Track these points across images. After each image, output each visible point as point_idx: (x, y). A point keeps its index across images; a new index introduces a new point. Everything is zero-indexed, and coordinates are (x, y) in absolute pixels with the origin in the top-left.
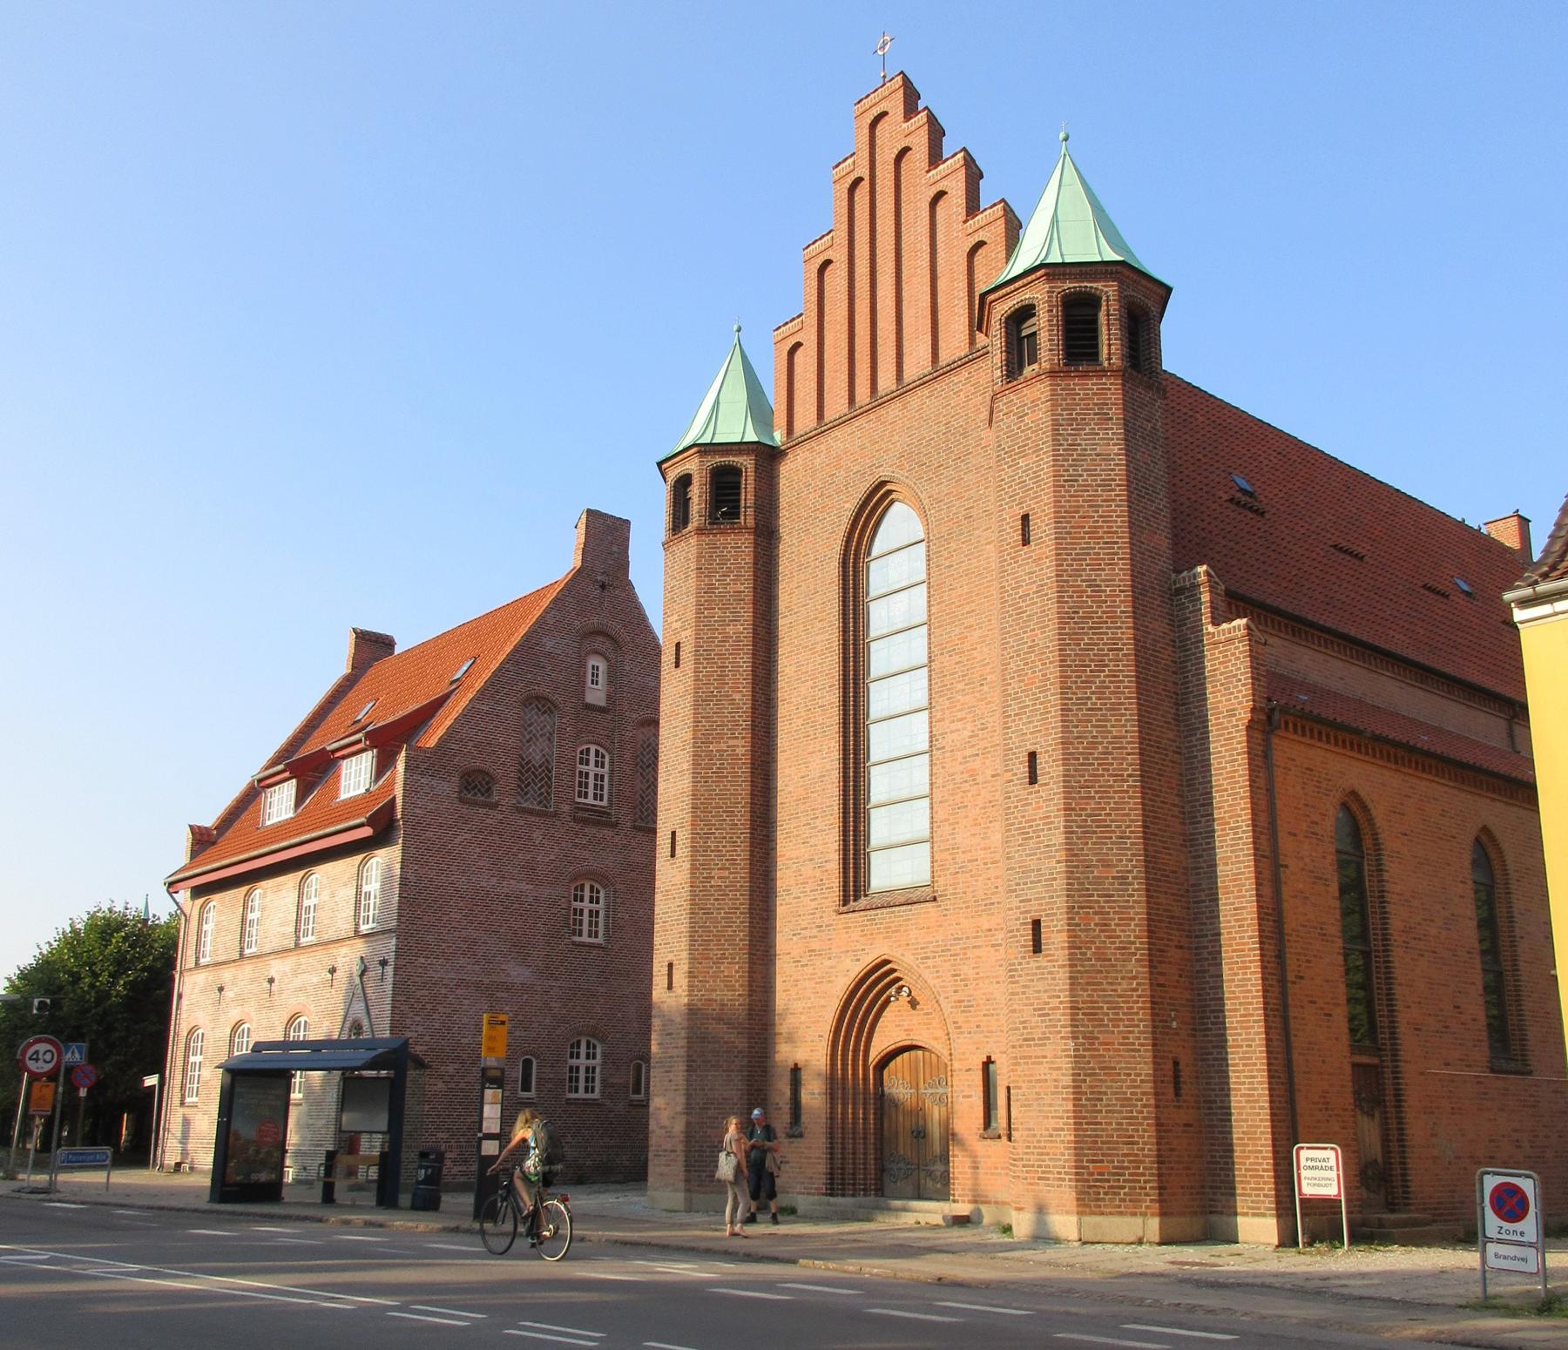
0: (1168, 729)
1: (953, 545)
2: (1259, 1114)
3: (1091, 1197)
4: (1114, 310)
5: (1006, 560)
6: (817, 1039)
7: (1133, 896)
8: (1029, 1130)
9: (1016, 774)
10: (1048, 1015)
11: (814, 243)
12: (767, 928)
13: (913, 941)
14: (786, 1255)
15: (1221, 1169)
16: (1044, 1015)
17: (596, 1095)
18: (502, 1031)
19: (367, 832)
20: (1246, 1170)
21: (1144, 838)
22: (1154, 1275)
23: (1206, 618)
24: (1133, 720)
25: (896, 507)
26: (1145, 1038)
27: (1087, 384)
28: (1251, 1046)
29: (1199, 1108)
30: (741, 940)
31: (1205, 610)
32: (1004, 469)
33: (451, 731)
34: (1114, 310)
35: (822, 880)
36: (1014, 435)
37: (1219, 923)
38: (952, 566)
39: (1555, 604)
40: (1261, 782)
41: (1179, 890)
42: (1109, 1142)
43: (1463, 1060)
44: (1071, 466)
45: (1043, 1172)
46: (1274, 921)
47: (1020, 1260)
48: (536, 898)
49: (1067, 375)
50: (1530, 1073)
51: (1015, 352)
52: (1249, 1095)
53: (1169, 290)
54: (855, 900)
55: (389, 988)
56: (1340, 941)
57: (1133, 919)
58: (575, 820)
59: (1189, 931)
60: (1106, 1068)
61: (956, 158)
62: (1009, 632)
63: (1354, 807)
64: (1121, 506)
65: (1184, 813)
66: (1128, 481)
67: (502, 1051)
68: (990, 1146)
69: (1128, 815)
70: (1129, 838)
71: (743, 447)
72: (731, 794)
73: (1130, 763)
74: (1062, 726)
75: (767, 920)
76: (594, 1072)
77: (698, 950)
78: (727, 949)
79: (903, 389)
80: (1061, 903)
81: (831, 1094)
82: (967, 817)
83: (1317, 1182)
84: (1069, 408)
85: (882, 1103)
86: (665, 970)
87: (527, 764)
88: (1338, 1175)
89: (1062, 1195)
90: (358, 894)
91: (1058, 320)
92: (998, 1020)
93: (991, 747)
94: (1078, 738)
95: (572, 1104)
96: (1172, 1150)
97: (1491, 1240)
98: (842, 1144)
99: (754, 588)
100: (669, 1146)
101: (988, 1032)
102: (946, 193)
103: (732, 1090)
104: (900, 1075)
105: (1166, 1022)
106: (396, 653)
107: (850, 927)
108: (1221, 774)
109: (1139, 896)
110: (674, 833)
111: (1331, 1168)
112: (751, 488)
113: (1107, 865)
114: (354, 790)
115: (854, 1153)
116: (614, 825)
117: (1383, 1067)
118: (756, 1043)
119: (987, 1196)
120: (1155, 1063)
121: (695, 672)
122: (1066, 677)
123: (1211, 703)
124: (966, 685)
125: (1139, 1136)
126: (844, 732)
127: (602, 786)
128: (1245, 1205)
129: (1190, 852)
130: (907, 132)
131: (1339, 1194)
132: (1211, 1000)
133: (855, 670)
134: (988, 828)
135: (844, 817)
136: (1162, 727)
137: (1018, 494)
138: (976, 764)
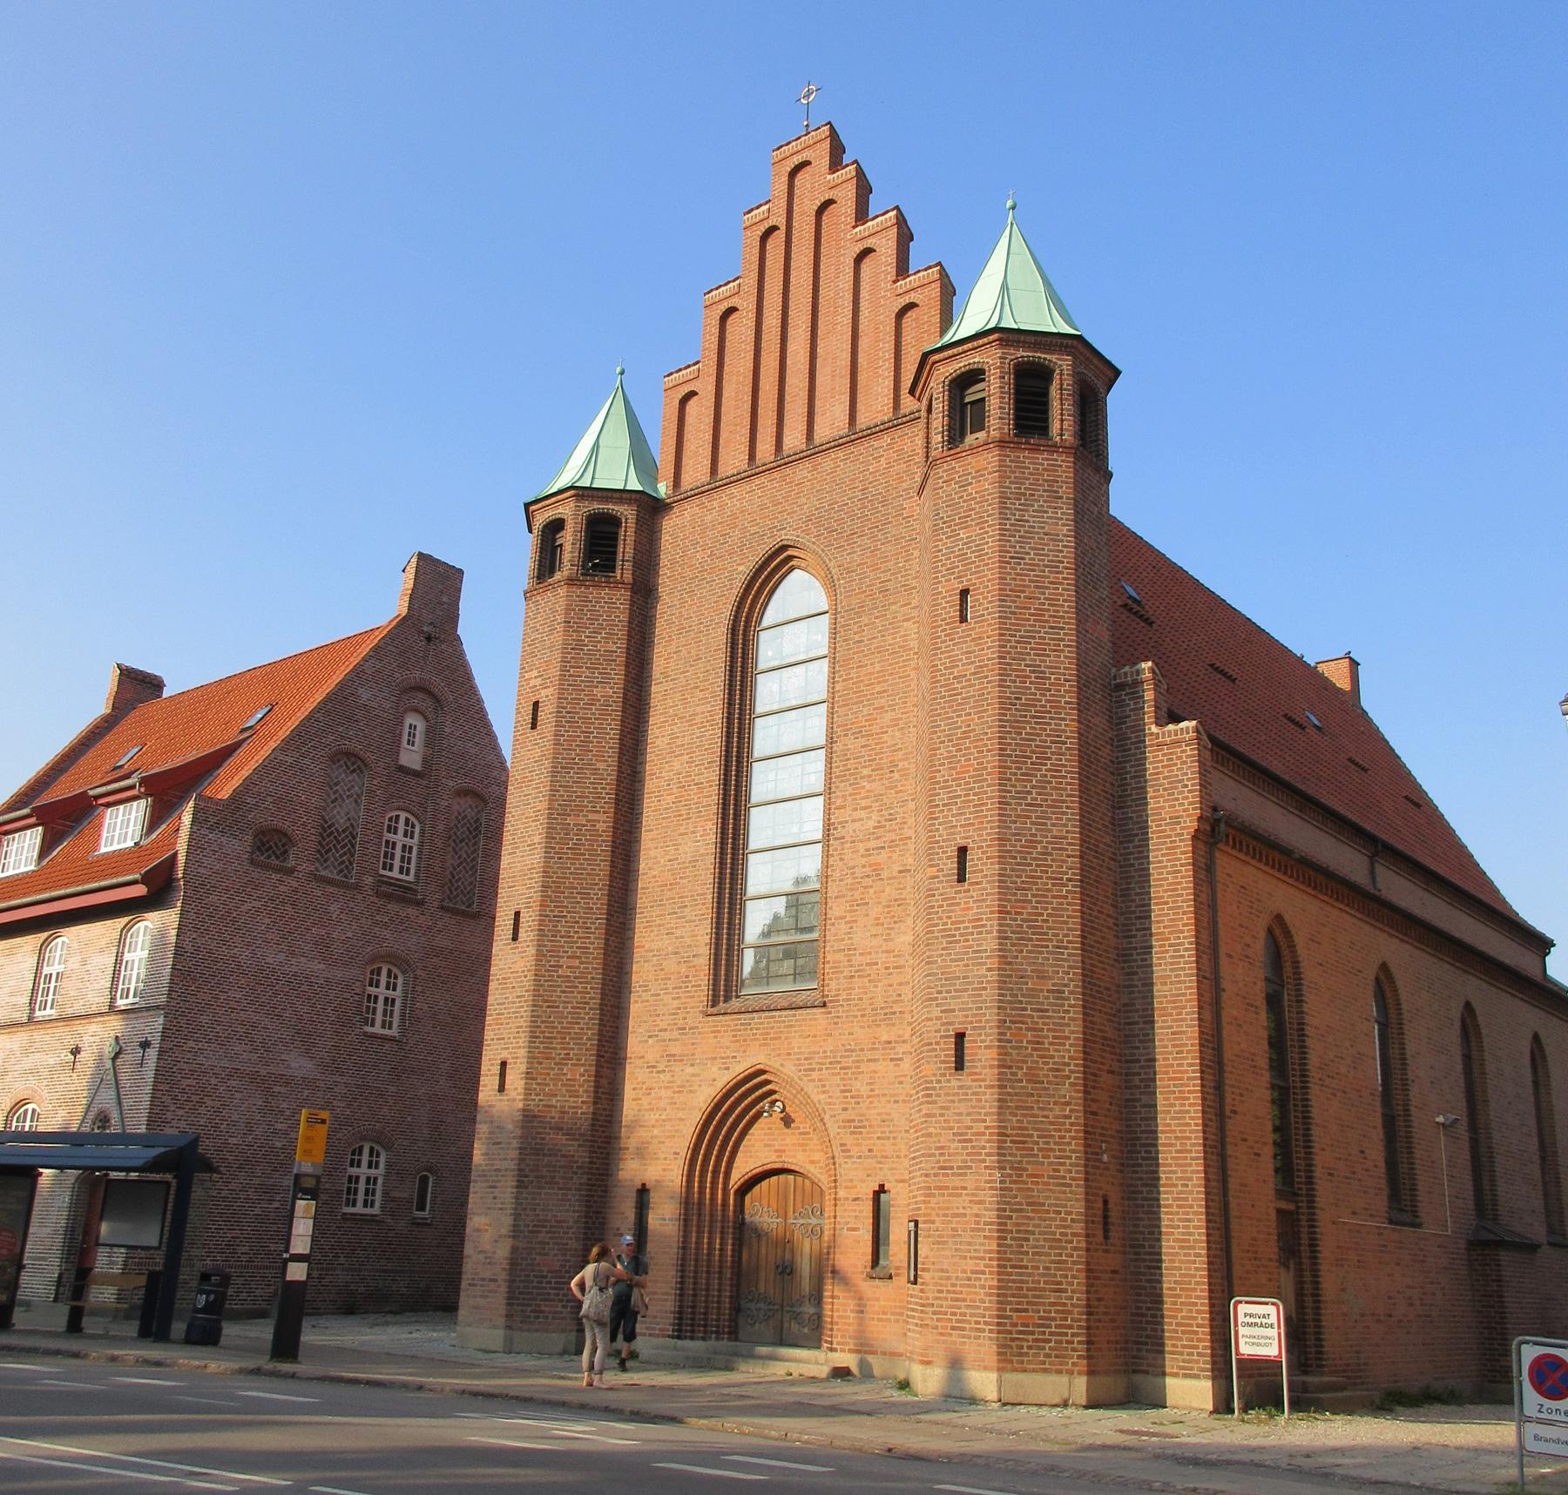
1: (865, 620)
2: (1195, 1262)
3: (1011, 1355)
4: (1068, 385)
5: (939, 637)
6: (672, 1157)
7: (1068, 1012)
8: (942, 1271)
12: (617, 1028)
15: (1147, 1322)
16: (965, 1141)
17: (376, 1210)
18: (323, 1130)
19: (140, 890)
20: (1177, 1324)
23: (1149, 718)
25: (797, 574)
27: (1038, 459)
28: (1187, 1186)
30: (588, 1039)
31: (1149, 709)
33: (248, 784)
35: (687, 977)
37: (1154, 1047)
40: (1203, 898)
41: (1111, 1008)
42: (1035, 1289)
43: (1366, 1209)
44: (1018, 542)
46: (1213, 1049)
47: (948, 1424)
48: (327, 980)
49: (1017, 446)
50: (1419, 1226)
51: (958, 418)
53: (1117, 373)
54: (725, 1002)
55: (150, 1074)
57: (1069, 1038)
58: (378, 894)
59: (1120, 1055)
61: (887, 216)
62: (939, 715)
63: (1277, 932)
66: (1076, 564)
67: (319, 1156)
69: (1066, 923)
71: (624, 496)
73: (1070, 867)
74: (1000, 821)
77: (538, 1048)
78: (573, 1049)
79: (813, 450)
80: (990, 1016)
81: (685, 1220)
82: (867, 915)
83: (1255, 1340)
85: (742, 1230)
86: (497, 1069)
87: (330, 827)
89: (981, 1348)
90: (118, 961)
91: (1009, 388)
94: (1016, 834)
95: (348, 1219)
97: (1529, 1420)
100: (487, 1275)
101: (883, 1157)
102: (875, 251)
103: (567, 1211)
104: (765, 1202)
106: (164, 696)
107: (719, 1032)
108: (1162, 885)
109: (1075, 1012)
110: (517, 914)
111: (1272, 1326)
112: (630, 540)
113: (1042, 977)
114: (119, 843)
115: (707, 1290)
116: (420, 903)
119: (872, 1346)
120: (1087, 1201)
122: (1004, 767)
123: (1152, 809)
124: (873, 771)
128: (1175, 1364)
130: (832, 184)
134: (893, 929)
137: (958, 567)
138: (882, 857)
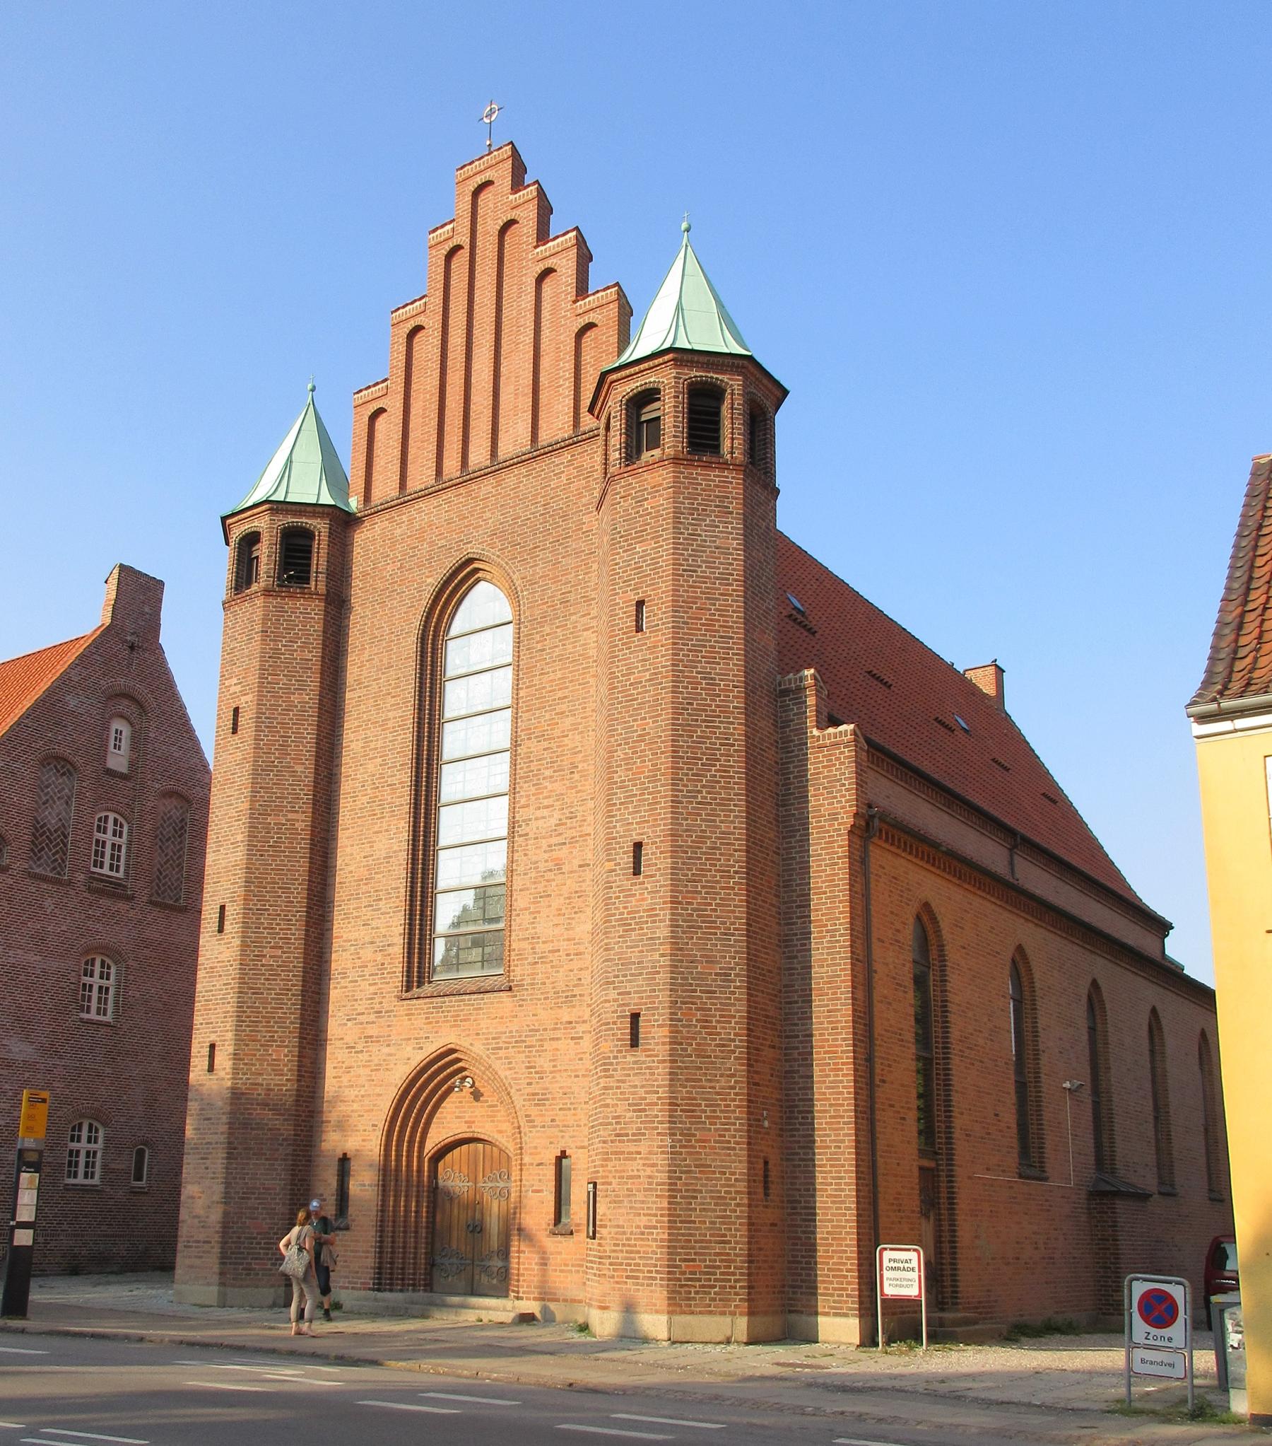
0: (770, 829)
1: (547, 629)
2: (845, 1215)
4: (738, 404)
8: (618, 1226)
9: (619, 864)
10: (645, 1110)
11: (404, 307)
12: (318, 1012)
13: (484, 1031)
14: (369, 1357)
16: (640, 1111)
17: (96, 1181)
21: (748, 936)
22: (763, 1378)
23: (811, 722)
24: (742, 817)
25: (482, 585)
26: (741, 1137)
27: (710, 475)
28: (840, 1147)
29: (783, 1208)
31: (811, 713)
32: (619, 553)
34: (738, 404)
36: (630, 519)
38: (544, 650)
39: (1236, 721)
41: (773, 989)
42: (702, 1241)
45: (632, 1271)
46: (865, 1025)
50: (1046, 1179)
52: (836, 1196)
53: (785, 393)
54: (418, 987)
56: (913, 1047)
58: (90, 890)
59: (781, 1031)
60: (703, 1166)
61: (567, 237)
63: (925, 918)
64: (737, 601)
65: (779, 914)
67: (41, 1133)
68: (561, 1242)
69: (734, 912)
70: (733, 935)
72: (288, 870)
73: (737, 862)
75: (319, 1003)
76: (94, 1156)
77: (245, 1031)
78: (277, 1032)
79: (496, 466)
80: (663, 997)
83: (898, 1282)
84: (692, 498)
85: (436, 1195)
86: (206, 1051)
87: (42, 827)
88: (920, 1276)
89: (659, 1295)
91: (683, 408)
92: (574, 1115)
93: (580, 836)
94: (687, 830)
96: (760, 1249)
98: (393, 1237)
99: (323, 657)
100: (202, 1237)
101: (565, 1126)
104: (456, 1167)
105: (759, 1120)
110: (223, 908)
111: (913, 1269)
112: (323, 553)
113: (711, 961)
115: (404, 1247)
116: (130, 898)
117: (938, 1170)
118: (302, 1130)
119: (555, 1294)
120: (749, 1162)
121: (256, 740)
123: (813, 806)
124: (554, 772)
125: (731, 1236)
126: (415, 813)
127: (119, 857)
129: (784, 953)
130: (514, 204)
131: (920, 1295)
132: (800, 1100)
133: (429, 750)
134: (573, 918)
135: (411, 901)
136: (765, 826)
138: (564, 852)
